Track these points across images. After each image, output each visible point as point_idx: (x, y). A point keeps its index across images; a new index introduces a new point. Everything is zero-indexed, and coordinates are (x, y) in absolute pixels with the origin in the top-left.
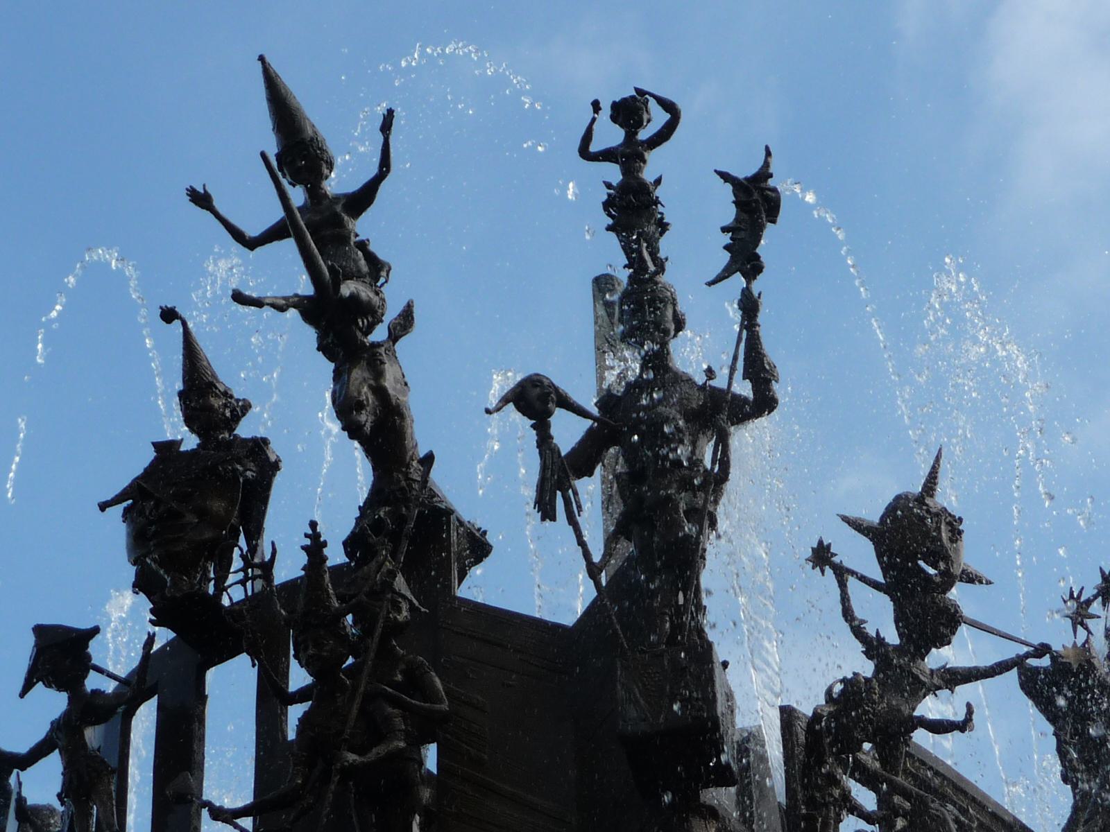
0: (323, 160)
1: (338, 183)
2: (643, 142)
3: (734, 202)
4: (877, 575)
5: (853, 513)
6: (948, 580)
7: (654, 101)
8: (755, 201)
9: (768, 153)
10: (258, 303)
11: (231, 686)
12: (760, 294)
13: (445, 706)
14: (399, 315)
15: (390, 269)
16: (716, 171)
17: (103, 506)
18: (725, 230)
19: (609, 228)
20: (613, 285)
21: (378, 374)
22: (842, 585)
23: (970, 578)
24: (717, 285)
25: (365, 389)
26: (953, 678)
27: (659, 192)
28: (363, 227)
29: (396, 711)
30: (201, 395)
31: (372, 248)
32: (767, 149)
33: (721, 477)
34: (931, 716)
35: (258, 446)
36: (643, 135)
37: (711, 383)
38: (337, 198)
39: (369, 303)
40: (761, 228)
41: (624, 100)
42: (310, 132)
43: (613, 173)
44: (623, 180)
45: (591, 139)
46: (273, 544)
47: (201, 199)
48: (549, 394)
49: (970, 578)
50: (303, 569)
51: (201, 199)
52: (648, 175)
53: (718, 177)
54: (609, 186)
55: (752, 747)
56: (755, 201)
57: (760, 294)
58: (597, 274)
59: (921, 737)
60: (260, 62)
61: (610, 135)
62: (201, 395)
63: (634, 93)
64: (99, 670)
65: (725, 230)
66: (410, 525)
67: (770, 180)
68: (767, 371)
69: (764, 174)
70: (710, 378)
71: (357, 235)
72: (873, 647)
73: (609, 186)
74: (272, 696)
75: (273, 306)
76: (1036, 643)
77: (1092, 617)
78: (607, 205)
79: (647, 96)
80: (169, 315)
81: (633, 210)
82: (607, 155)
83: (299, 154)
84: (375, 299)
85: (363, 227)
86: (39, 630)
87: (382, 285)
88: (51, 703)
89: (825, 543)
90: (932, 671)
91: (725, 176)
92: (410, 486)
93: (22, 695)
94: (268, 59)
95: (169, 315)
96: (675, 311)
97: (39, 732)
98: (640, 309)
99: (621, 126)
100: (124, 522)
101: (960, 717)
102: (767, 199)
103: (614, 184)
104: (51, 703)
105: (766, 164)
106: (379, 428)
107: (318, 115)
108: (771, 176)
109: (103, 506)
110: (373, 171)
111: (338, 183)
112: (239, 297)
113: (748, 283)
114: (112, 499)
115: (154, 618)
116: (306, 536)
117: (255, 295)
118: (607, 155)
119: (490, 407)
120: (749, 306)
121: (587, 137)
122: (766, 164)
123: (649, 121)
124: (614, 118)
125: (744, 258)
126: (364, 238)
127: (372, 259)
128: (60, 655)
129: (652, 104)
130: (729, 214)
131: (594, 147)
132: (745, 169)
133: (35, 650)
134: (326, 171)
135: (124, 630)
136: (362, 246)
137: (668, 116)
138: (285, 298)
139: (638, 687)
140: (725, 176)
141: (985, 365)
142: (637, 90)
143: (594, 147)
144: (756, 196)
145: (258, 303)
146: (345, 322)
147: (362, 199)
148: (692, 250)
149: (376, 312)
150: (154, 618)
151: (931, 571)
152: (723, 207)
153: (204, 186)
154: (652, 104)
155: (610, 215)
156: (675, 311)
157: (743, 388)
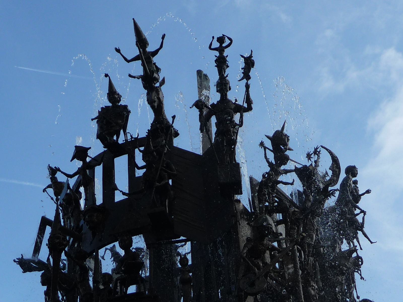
0: (147, 44)
1: (150, 49)
2: (224, 47)
3: (244, 62)
4: (271, 148)
5: (267, 135)
6: (286, 149)
7: (227, 38)
8: (249, 63)
9: (252, 52)
10: (134, 77)
11: (121, 163)
12: (250, 84)
13: (175, 173)
14: (162, 80)
15: (161, 70)
16: (240, 55)
17: (92, 120)
18: (242, 69)
19: (216, 66)
20: (201, 73)
21: (158, 94)
22: (265, 151)
23: (290, 149)
24: (241, 81)
25: (156, 97)
26: (286, 172)
27: (227, 59)
28: (155, 59)
29: (166, 174)
30: (113, 95)
31: (156, 64)
32: (251, 50)
33: (241, 124)
34: (284, 181)
35: (125, 107)
36: (224, 45)
37: (236, 103)
38: (149, 52)
39: (157, 78)
40: (251, 69)
41: (220, 37)
42: (144, 37)
44: (219, 56)
45: (212, 45)
46: (138, 133)
47: (118, 51)
48: (203, 104)
49: (290, 149)
51: (118, 51)
52: (225, 54)
53: (241, 56)
54: (216, 56)
56: (249, 63)
57: (250, 84)
58: (198, 70)
59: (280, 186)
60: (133, 20)
61: (216, 44)
62: (113, 95)
63: (222, 36)
64: (89, 156)
65: (242, 69)
66: (162, 129)
67: (252, 58)
68: (251, 102)
69: (251, 56)
70: (236, 102)
71: (153, 61)
72: (270, 164)
73: (216, 56)
74: (132, 165)
75: (137, 78)
76: (304, 165)
77: (312, 158)
78: (216, 61)
79: (225, 36)
80: (106, 75)
81: (221, 63)
82: (215, 49)
83: (141, 42)
84: (158, 77)
85: (155, 59)
86: (76, 147)
87: (159, 73)
88: (78, 164)
89: (263, 141)
90: (282, 170)
91: (242, 56)
92: (163, 120)
93: (71, 161)
94: (135, 19)
95: (106, 75)
96: (229, 86)
97: (76, 170)
98: (223, 86)
99: (219, 43)
100: (97, 123)
101: (291, 181)
102: (251, 62)
103: (217, 56)
104: (78, 164)
105: (251, 54)
106: (157, 106)
107: (146, 34)
108: (252, 57)
109: (92, 120)
110: (159, 47)
111: (150, 49)
112: (130, 76)
113: (247, 81)
114: (94, 118)
115: (104, 146)
116: (147, 133)
117: (134, 75)
118: (215, 49)
119: (191, 107)
120: (247, 86)
122: (251, 54)
123: (225, 42)
124: (218, 41)
125: (246, 76)
126: (155, 62)
127: (156, 67)
128: (80, 153)
129: (226, 38)
130: (243, 65)
131: (212, 47)
132: (247, 55)
133: (75, 151)
134: (147, 46)
135: (96, 148)
136: (155, 64)
137: (230, 41)
138: (139, 76)
139: (223, 172)
140: (242, 56)
142: (223, 35)
143: (212, 47)
144: (249, 61)
145: (134, 77)
146: (151, 81)
147: (155, 53)
148: (234, 72)
149: (158, 80)
150: (104, 146)
151: (283, 148)
152: (241, 63)
153: (119, 47)
154: (226, 38)
155: (216, 63)
156: (229, 86)
157: (246, 105)
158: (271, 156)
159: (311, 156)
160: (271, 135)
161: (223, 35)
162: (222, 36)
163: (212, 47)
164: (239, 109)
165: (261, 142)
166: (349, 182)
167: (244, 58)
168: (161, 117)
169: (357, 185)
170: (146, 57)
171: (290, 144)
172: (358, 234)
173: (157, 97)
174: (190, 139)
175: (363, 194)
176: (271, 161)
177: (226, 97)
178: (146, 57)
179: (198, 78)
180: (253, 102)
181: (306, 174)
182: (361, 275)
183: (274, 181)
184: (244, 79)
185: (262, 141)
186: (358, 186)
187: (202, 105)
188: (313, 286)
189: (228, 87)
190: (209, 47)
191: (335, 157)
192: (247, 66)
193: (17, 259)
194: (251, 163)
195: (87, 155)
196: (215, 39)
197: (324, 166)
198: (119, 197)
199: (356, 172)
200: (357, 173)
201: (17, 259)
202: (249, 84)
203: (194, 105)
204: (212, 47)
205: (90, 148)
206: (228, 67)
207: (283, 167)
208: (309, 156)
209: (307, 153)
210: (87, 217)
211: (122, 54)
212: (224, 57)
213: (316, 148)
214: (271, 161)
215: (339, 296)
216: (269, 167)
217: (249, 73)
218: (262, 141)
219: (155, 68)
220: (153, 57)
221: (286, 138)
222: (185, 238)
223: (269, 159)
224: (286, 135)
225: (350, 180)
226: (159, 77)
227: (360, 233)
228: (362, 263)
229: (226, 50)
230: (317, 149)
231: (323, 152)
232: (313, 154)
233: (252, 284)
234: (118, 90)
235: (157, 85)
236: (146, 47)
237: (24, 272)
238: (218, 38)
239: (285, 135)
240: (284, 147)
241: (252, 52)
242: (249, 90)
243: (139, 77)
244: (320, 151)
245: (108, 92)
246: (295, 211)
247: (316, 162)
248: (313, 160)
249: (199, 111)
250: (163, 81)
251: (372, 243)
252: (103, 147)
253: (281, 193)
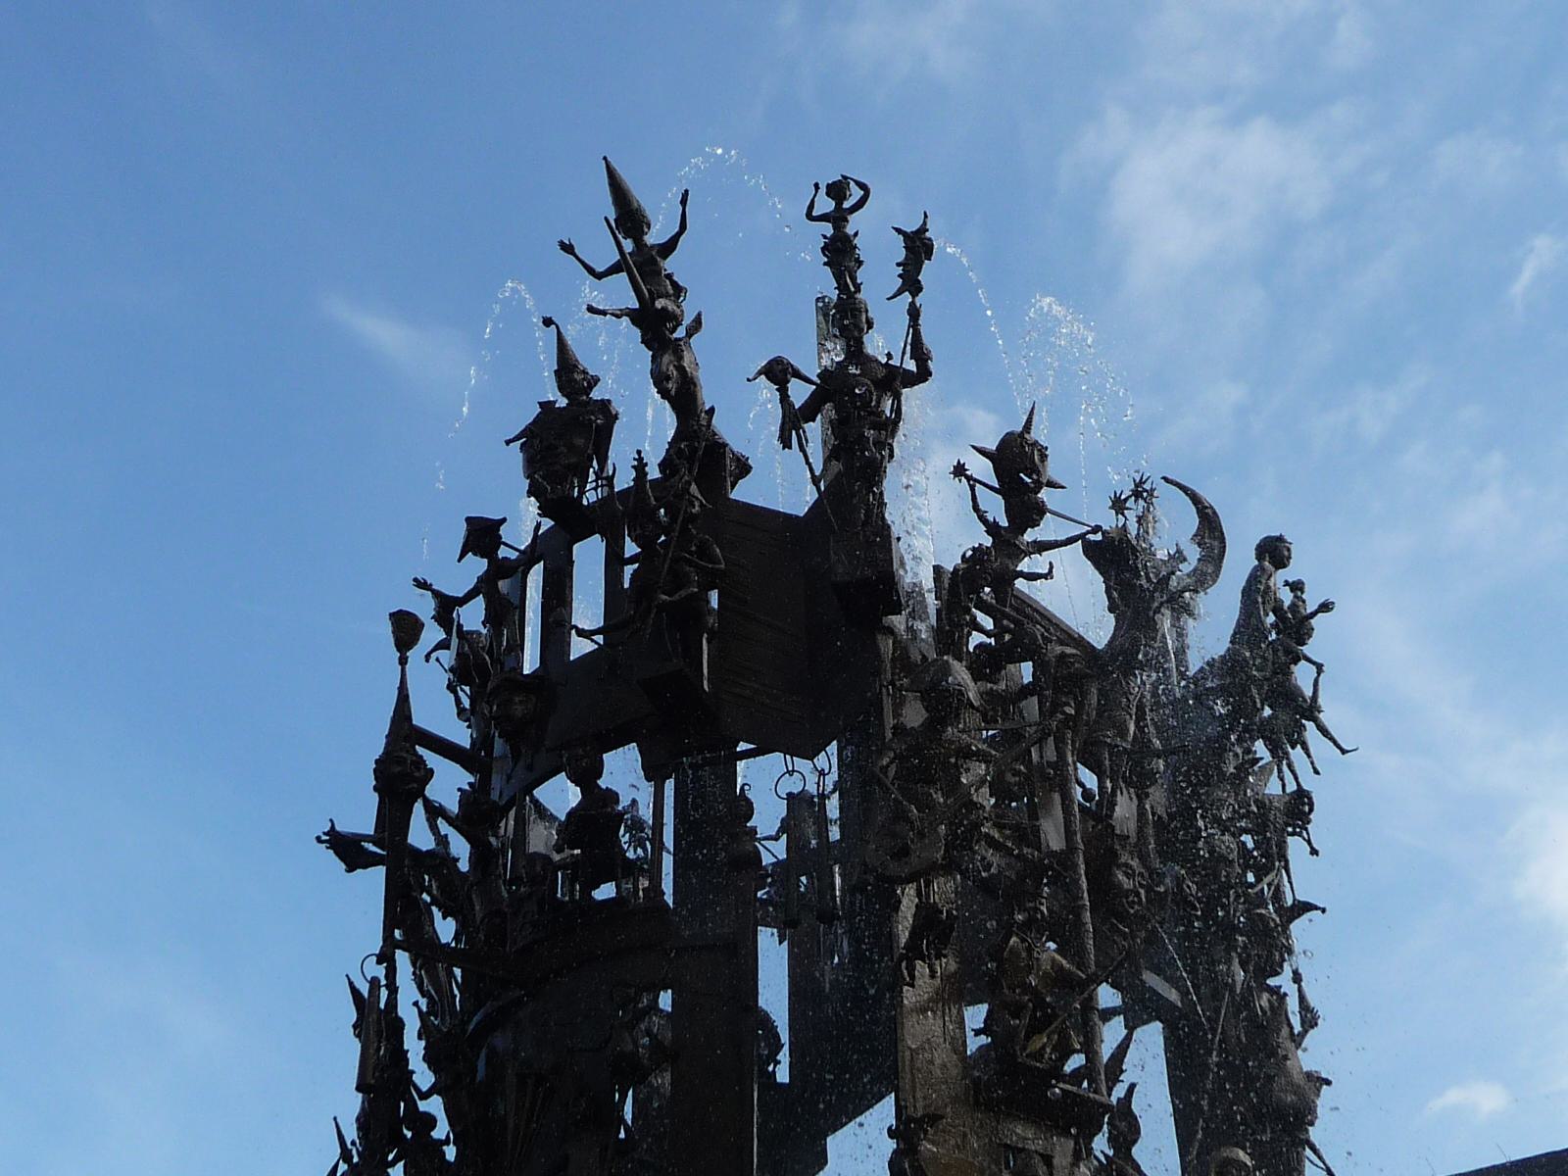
1: (654, 237)
6: (1039, 486)
8: (918, 247)
9: (926, 216)
10: (604, 313)
11: (589, 556)
17: (508, 442)
19: (825, 264)
21: (680, 358)
23: (1051, 484)
25: (671, 368)
28: (669, 265)
30: (569, 372)
36: (846, 205)
41: (834, 183)
43: (828, 229)
46: (614, 464)
47: (568, 248)
51: (568, 248)
52: (850, 230)
54: (825, 237)
56: (918, 247)
61: (825, 205)
62: (569, 372)
63: (840, 178)
69: (923, 229)
71: (665, 270)
72: (992, 528)
73: (825, 237)
74: (614, 561)
75: (613, 314)
76: (1093, 525)
77: (1127, 509)
81: (840, 253)
83: (629, 219)
84: (678, 311)
85: (669, 265)
88: (478, 565)
89: (962, 462)
94: (609, 159)
95: (548, 322)
96: (867, 317)
98: (845, 317)
102: (925, 244)
103: (828, 236)
104: (478, 565)
105: (925, 223)
106: (682, 394)
107: (643, 196)
108: (927, 230)
111: (654, 237)
119: (751, 378)
120: (914, 313)
122: (925, 223)
124: (828, 194)
125: (911, 283)
127: (675, 284)
128: (482, 535)
129: (852, 184)
130: (901, 255)
131: (815, 213)
135: (524, 521)
136: (669, 277)
142: (842, 176)
143: (815, 213)
146: (658, 325)
148: (878, 278)
154: (852, 184)
155: (825, 255)
156: (867, 317)
157: (911, 365)
158: (996, 508)
159: (1127, 505)
160: (992, 445)
161: (842, 176)
162: (840, 178)
163: (814, 214)
164: (894, 380)
165: (955, 464)
166: (1264, 581)
167: (904, 236)
168: (695, 423)
169: (1302, 593)
171: (1052, 470)
172: (1305, 730)
173: (674, 366)
174: (782, 481)
175: (1313, 614)
176: (994, 519)
177: (861, 348)
179: (821, 318)
180: (933, 354)
181: (1113, 556)
182: (1309, 842)
184: (903, 292)
185: (959, 462)
187: (785, 371)
188: (1126, 865)
189: (864, 320)
190: (807, 215)
191: (1207, 507)
192: (912, 256)
193: (324, 834)
194: (932, 522)
195: (498, 542)
196: (823, 190)
197: (1171, 533)
198: (580, 647)
199: (1286, 553)
200: (1290, 554)
201: (324, 834)
202: (918, 305)
203: (760, 373)
204: (814, 214)
205: (504, 520)
206: (860, 263)
207: (1030, 535)
208: (1119, 505)
209: (1113, 496)
210: (495, 708)
211: (580, 256)
212: (847, 236)
213: (1138, 481)
214: (994, 519)
215: (1188, 887)
216: (988, 534)
217: (918, 275)
218: (959, 462)
219: (670, 287)
220: (665, 258)
221: (1036, 452)
222: (753, 746)
223: (986, 512)
224: (1035, 444)
225: (1266, 577)
226: (682, 311)
227: (1310, 725)
228: (1311, 810)
229: (852, 218)
230: (1144, 483)
231: (1163, 491)
232: (1133, 498)
233: (903, 853)
235: (680, 333)
236: (644, 233)
237: (350, 869)
238: (828, 186)
239: (1032, 445)
240: (1030, 478)
241: (926, 216)
242: (920, 322)
243: (619, 312)
244: (1152, 490)
245: (556, 368)
246: (1063, 655)
247: (1140, 520)
248: (1132, 516)
249: (777, 389)
250: (697, 323)
251: (1344, 752)
252: (538, 514)
253: (1036, 610)
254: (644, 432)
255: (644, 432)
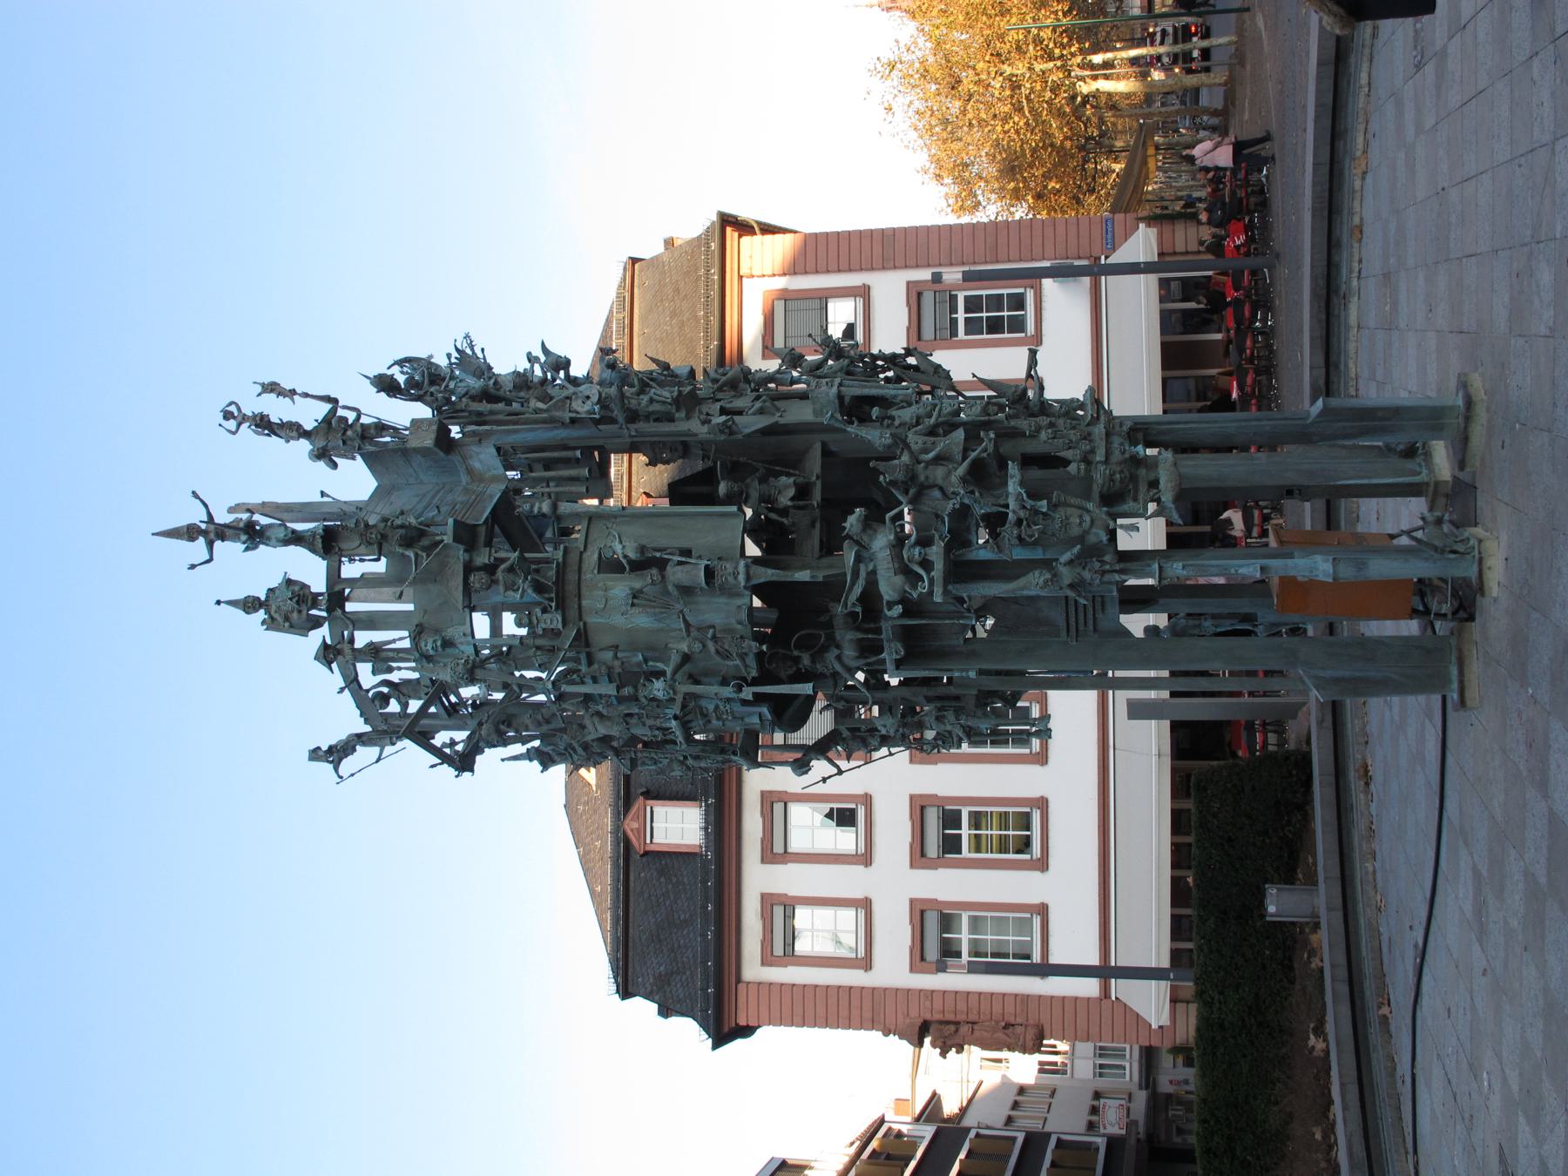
8: (272, 388)
30: (249, 605)
47: (193, 567)
50: (354, 458)
51: (193, 567)
55: (482, 456)
56: (272, 388)
61: (232, 424)
66: (332, 535)
69: (263, 385)
82: (239, 425)
83: (190, 533)
98: (291, 430)
107: (182, 521)
118: (239, 425)
120: (306, 395)
121: (744, 228)
130: (273, 395)
132: (259, 389)
141: (496, 628)
148: (279, 409)
170: (214, 533)
178: (214, 533)
183: (1062, 147)
186: (325, 748)
196: (225, 423)
234: (241, 596)
254: (311, 570)
255: (311, 570)
